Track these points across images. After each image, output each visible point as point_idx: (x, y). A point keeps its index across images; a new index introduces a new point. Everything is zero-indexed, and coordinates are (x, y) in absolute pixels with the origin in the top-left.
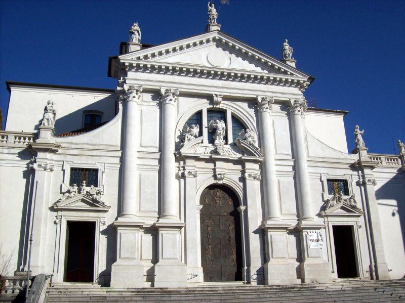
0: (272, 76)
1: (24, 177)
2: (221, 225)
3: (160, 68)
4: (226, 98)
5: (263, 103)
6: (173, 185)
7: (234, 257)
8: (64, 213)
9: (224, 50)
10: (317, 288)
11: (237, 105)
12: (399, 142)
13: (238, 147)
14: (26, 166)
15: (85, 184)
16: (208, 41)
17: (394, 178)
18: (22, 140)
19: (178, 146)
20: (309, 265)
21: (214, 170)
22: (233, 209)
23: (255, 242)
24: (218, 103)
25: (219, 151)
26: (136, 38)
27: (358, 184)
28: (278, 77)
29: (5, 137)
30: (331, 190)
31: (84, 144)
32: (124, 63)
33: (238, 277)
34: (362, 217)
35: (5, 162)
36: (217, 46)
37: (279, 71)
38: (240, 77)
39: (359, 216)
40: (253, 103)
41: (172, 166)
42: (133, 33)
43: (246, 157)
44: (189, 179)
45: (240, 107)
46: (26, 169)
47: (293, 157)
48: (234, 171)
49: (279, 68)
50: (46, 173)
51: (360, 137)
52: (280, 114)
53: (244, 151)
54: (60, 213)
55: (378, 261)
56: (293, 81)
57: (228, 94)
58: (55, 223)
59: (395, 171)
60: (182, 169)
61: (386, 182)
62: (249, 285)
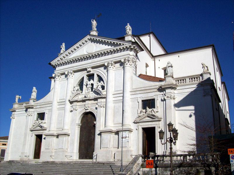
0: (115, 49)
4: (93, 68)
8: (140, 124)
10: (116, 164)
17: (194, 91)
28: (118, 48)
29: (184, 80)
52: (120, 68)
57: (93, 66)
58: (137, 130)
59: (195, 86)
61: (187, 95)
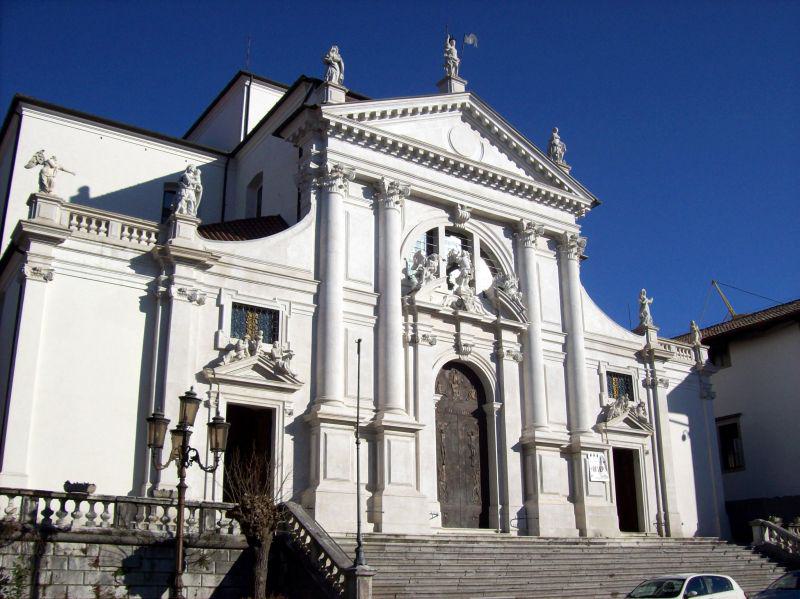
0: (536, 186)
1: (142, 309)
2: (460, 432)
3: (384, 141)
4: (477, 215)
5: (335, 175)
6: (398, 353)
7: (478, 487)
8: (223, 388)
9: (473, 128)
11: (488, 228)
12: (692, 324)
13: (491, 301)
14: (146, 287)
15: (262, 337)
16: (454, 108)
18: (144, 236)
19: (409, 289)
20: (592, 508)
21: (457, 336)
22: (476, 407)
23: (514, 461)
24: (463, 220)
25: (468, 305)
26: (336, 75)
27: (645, 384)
30: (238, 329)
31: (253, 260)
32: (328, 121)
33: (484, 522)
34: (649, 438)
35: (106, 274)
36: (464, 119)
37: (551, 181)
38: (369, 139)
39: (646, 436)
40: (513, 229)
41: (397, 321)
42: (329, 64)
43: (503, 321)
44: (423, 348)
45: (492, 232)
46: (146, 294)
47: (377, 290)
48: (484, 342)
49: (554, 177)
50: (193, 306)
51: (647, 308)
53: (499, 308)
54: (215, 387)
55: (670, 509)
56: (362, 133)
57: (480, 208)
59: (688, 369)
60: (411, 328)
62: (504, 535)
